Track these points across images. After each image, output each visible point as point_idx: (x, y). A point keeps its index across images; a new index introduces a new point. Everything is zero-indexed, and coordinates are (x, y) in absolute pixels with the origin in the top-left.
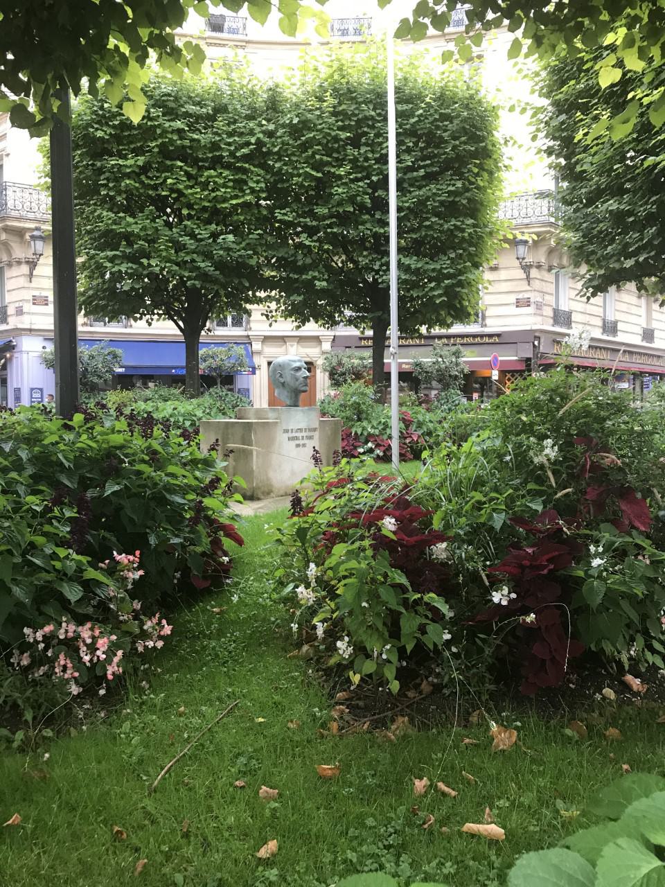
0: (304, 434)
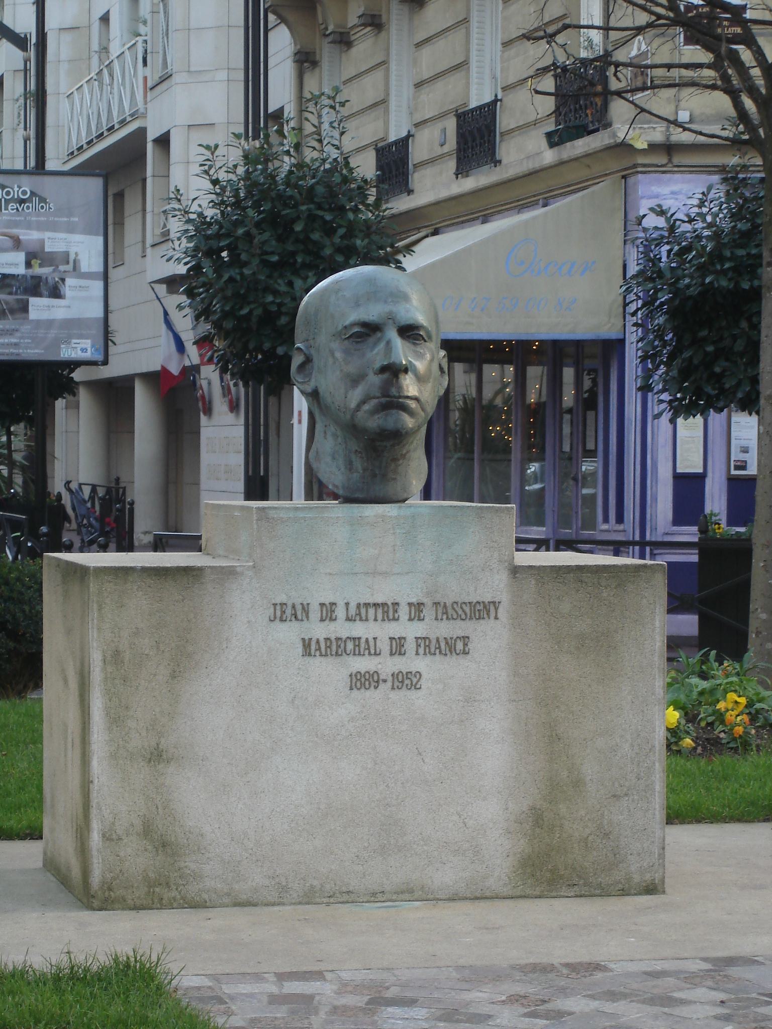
0: (412, 630)
